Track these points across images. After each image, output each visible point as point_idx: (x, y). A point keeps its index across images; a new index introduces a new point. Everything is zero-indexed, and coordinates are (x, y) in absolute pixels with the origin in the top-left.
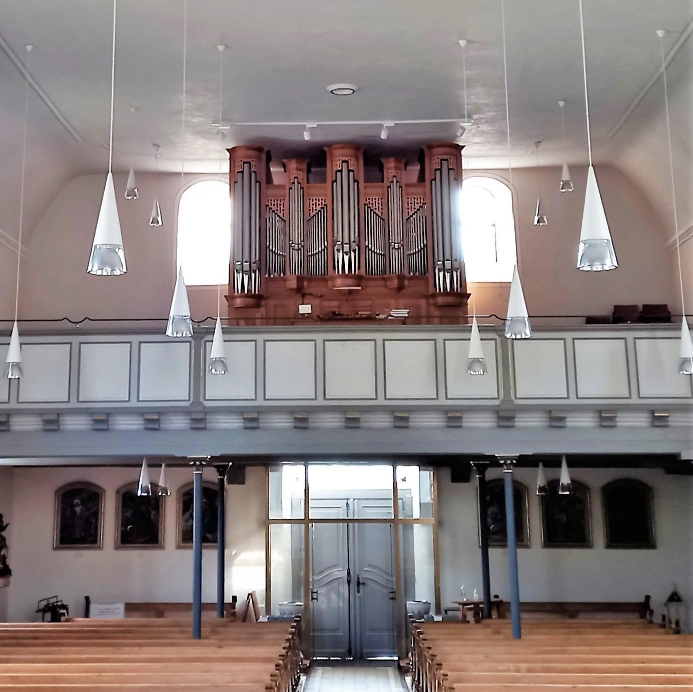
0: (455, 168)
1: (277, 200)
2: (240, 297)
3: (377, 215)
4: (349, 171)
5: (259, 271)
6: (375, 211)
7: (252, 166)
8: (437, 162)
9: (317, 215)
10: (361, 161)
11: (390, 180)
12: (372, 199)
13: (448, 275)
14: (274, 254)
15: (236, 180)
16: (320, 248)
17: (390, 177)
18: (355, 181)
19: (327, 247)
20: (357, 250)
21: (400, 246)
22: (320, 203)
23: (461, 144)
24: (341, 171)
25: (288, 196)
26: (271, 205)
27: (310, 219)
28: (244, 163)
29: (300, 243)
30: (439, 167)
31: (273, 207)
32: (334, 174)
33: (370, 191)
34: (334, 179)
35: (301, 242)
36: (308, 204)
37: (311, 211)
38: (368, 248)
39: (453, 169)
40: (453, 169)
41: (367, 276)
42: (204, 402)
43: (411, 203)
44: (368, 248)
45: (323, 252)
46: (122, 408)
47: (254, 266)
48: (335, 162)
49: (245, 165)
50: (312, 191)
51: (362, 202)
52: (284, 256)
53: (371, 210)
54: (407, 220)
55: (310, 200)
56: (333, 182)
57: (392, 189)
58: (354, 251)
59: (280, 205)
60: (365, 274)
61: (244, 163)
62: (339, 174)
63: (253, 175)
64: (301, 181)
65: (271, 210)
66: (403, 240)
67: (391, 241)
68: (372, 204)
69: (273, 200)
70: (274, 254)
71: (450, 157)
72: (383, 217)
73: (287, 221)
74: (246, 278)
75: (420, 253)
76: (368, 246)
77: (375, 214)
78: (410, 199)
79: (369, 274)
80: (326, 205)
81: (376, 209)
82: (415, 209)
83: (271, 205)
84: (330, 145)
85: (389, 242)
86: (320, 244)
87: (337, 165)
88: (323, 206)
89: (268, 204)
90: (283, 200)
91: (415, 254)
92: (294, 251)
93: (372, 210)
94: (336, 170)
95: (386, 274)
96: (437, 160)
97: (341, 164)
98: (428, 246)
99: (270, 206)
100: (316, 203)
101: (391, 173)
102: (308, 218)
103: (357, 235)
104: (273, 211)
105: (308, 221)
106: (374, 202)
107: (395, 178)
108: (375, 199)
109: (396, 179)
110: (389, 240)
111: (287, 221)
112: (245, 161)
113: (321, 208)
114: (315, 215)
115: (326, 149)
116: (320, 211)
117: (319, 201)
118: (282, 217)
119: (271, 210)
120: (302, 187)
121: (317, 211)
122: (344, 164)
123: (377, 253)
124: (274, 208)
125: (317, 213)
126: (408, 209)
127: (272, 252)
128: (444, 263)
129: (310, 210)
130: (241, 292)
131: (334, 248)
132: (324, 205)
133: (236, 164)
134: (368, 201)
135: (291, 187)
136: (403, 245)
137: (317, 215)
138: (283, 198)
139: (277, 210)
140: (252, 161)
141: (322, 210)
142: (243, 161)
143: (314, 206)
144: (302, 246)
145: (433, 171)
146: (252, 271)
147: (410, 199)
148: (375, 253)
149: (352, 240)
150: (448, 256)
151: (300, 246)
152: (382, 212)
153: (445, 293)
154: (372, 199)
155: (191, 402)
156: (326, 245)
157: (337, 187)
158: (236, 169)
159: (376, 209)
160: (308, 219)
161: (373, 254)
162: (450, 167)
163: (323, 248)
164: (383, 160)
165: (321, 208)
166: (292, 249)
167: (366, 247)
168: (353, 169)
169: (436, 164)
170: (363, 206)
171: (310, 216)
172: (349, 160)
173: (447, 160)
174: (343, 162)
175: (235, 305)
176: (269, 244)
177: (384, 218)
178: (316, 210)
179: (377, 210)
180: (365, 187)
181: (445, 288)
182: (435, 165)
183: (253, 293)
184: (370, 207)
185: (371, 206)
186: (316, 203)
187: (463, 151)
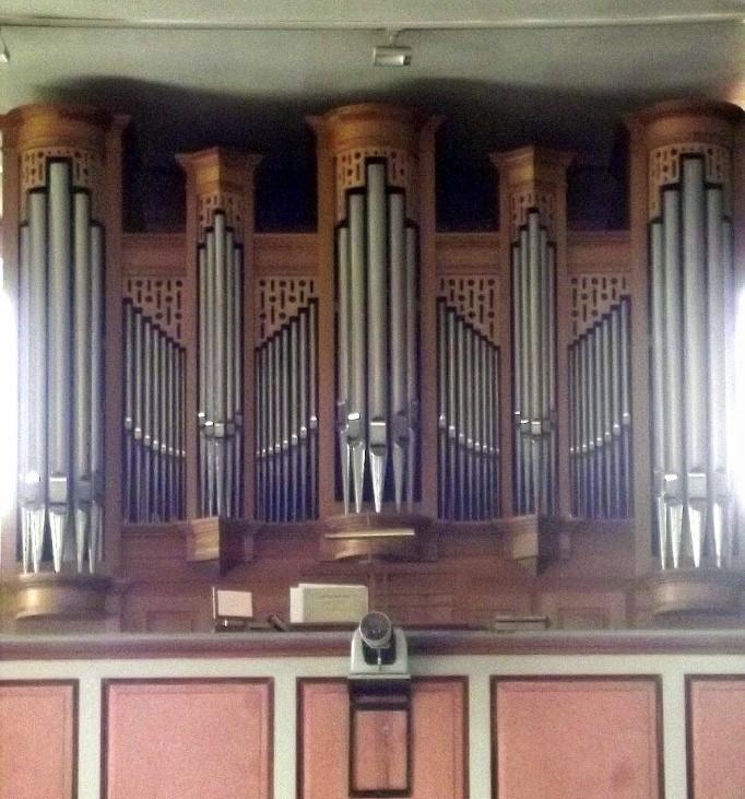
2: (37, 584)
5: (102, 506)
6: (468, 320)
7: (75, 172)
12: (462, 283)
13: (695, 517)
15: (23, 218)
16: (294, 436)
17: (204, 213)
18: (407, 223)
19: (631, 430)
20: (412, 440)
25: (191, 273)
26: (139, 300)
27: (265, 345)
28: (51, 160)
29: (229, 416)
32: (341, 202)
33: (454, 257)
34: (341, 216)
36: (258, 298)
39: (719, 187)
40: (719, 187)
43: (273, 299)
44: (133, 439)
47: (85, 489)
48: (346, 164)
50: (267, 257)
51: (431, 291)
52: (182, 459)
55: (263, 283)
58: (403, 441)
61: (369, 161)
62: (355, 201)
63: (80, 200)
66: (242, 412)
67: (201, 415)
69: (288, 285)
70: (148, 455)
71: (710, 146)
73: (506, 350)
74: (57, 524)
75: (286, 459)
76: (133, 431)
77: (148, 326)
80: (314, 301)
83: (139, 300)
84: (325, 104)
85: (513, 416)
88: (305, 305)
89: (128, 295)
91: (612, 445)
94: (347, 186)
95: (457, 519)
96: (670, 157)
98: (321, 432)
104: (146, 320)
110: (513, 409)
111: (506, 350)
116: (297, 319)
117: (149, 288)
119: (139, 316)
120: (238, 241)
121: (286, 321)
122: (370, 167)
124: (150, 309)
125: (288, 327)
128: (683, 480)
129: (263, 316)
131: (337, 434)
132: (311, 300)
133: (25, 164)
135: (201, 241)
144: (237, 427)
145: (341, 194)
146: (76, 505)
149: (397, 406)
150: (694, 457)
151: (231, 427)
153: (687, 573)
154: (462, 283)
157: (351, 239)
159: (159, 316)
160: (258, 344)
161: (462, 454)
167: (439, 430)
168: (401, 185)
171: (262, 335)
174: (369, 161)
175: (23, 609)
177: (497, 343)
179: (477, 318)
180: (439, 245)
183: (80, 569)
184: (454, 309)
185: (457, 304)
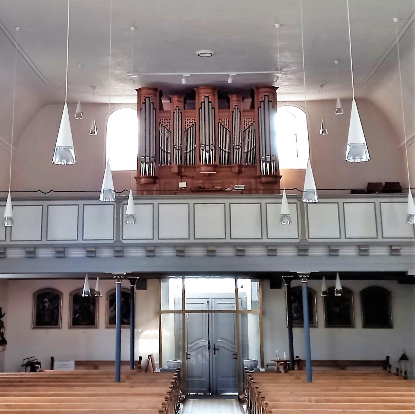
0: (272, 100)
1: (166, 120)
2: (144, 178)
3: (226, 128)
4: (209, 102)
5: (155, 162)
6: (224, 126)
7: (151, 100)
8: (262, 97)
9: (190, 129)
10: (216, 96)
11: (234, 108)
12: (223, 119)
13: (268, 165)
14: (164, 152)
15: (141, 108)
16: (192, 149)
17: (233, 106)
18: (212, 108)
19: (196, 148)
20: (214, 149)
21: (239, 147)
22: (192, 121)
23: (276, 86)
24: (204, 102)
25: (172, 117)
26: (162, 123)
27: (186, 131)
28: (146, 97)
29: (179, 145)
30: (263, 100)
31: (163, 124)
32: (200, 104)
33: (221, 114)
34: (200, 107)
35: (180, 145)
36: (185, 122)
37: (186, 126)
38: (221, 149)
39: (271, 101)
40: (271, 101)
41: (220, 165)
42: (122, 240)
43: (246, 122)
44: (221, 149)
45: (193, 151)
46: (73, 244)
47: (152, 159)
48: (201, 97)
49: (147, 98)
50: (187, 114)
51: (217, 121)
52: (170, 153)
53: (222, 126)
54: (244, 131)
55: (185, 119)
56: (199, 109)
57: (235, 113)
58: (212, 150)
59: (168, 123)
60: (218, 164)
61: (146, 97)
62: (203, 104)
63: (152, 104)
64: (180, 108)
65: (162, 126)
66: (241, 144)
67: (234, 144)
68: (223, 122)
69: (163, 120)
70: (164, 152)
71: (269, 94)
72: (229, 130)
73: (172, 132)
74: (147, 166)
75: (251, 151)
76: (220, 147)
77: (224, 128)
78: (245, 119)
79: (221, 164)
80: (195, 123)
81: (225, 125)
82: (248, 125)
83: (162, 123)
84: (198, 87)
85: (233, 145)
86: (192, 146)
87: (202, 99)
88: (193, 123)
89: (160, 122)
90: (170, 120)
91: (249, 152)
92: (176, 150)
93: (223, 126)
94: (201, 101)
95: (231, 164)
96: (262, 96)
97: (204, 98)
98: (256, 147)
99: (162, 124)
100: (189, 121)
101: (234, 103)
102: (185, 130)
103: (214, 141)
104: (163, 126)
105: (184, 132)
106: (224, 121)
107: (236, 107)
108: (225, 119)
109: (237, 107)
110: (233, 144)
111: (172, 132)
112: (147, 96)
113: (193, 124)
114: (188, 129)
115: (195, 89)
116: (192, 126)
117: (191, 120)
118: (169, 130)
119: (162, 126)
120: (181, 112)
121: (190, 127)
122: (206, 98)
123: (226, 151)
124: (164, 125)
125: (190, 128)
126: (245, 125)
127: (163, 151)
128: (266, 157)
129: (186, 126)
130: (144, 175)
131: (200, 148)
132: (194, 123)
133: (141, 98)
134: (220, 120)
135: (174, 112)
136: (241, 147)
137: (190, 129)
138: (169, 119)
139: (166, 126)
140: (151, 96)
141: (193, 126)
142: (145, 96)
143: (188, 123)
144: (181, 147)
145: (260, 102)
146: (151, 162)
147: (245, 119)
148: (224, 151)
149: (211, 143)
150: (268, 153)
151: (180, 147)
152: (229, 127)
153: (267, 175)
154: (223, 119)
155: (114, 240)
156: (195, 146)
157: (202, 112)
158: (141, 101)
159: (225, 125)
160: (185, 131)
161: (223, 152)
162: (270, 100)
163: (193, 148)
164: (229, 96)
165: (193, 124)
166: (175, 149)
167: (219, 148)
168: (211, 101)
169: (261, 98)
170: (217, 123)
171: (185, 129)
172: (209, 96)
173: (268, 96)
174: (205, 97)
175: (141, 182)
176: (161, 146)
177: (230, 130)
178: (189, 126)
179: (226, 125)
180: (219, 112)
181: (266, 173)
182: (261, 99)
183: (152, 175)
184: (221, 124)
185: (222, 123)
186: (189, 121)
187: (277, 90)
